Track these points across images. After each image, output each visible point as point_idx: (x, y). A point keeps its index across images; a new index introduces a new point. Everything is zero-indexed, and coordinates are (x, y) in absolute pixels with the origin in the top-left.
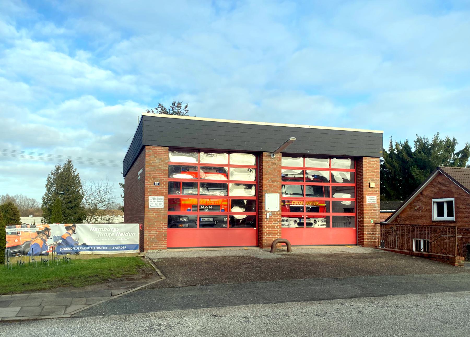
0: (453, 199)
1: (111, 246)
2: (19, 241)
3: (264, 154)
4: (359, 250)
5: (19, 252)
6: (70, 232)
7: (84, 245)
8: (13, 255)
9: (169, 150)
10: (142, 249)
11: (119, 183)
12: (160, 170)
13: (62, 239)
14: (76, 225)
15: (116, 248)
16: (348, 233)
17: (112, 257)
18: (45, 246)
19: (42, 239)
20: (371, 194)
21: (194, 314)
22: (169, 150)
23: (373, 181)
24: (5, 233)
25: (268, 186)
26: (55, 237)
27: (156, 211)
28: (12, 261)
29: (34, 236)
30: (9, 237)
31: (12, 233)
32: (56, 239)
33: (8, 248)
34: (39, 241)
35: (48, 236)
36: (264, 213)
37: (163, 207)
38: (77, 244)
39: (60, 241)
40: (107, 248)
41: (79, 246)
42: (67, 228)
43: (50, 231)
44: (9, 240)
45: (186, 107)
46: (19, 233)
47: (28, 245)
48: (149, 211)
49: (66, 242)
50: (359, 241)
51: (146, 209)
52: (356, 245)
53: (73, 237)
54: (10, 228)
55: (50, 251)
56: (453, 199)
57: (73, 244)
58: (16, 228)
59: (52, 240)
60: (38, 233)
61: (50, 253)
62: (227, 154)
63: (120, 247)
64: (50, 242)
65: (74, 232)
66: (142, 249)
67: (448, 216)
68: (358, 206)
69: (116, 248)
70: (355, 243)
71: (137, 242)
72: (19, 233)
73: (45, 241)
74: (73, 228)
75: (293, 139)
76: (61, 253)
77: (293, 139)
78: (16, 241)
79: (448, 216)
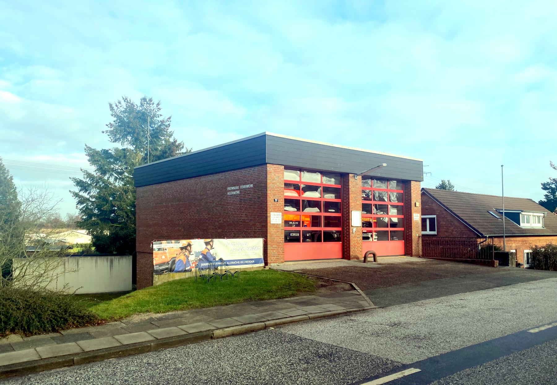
0: (435, 216)
1: (237, 260)
2: (166, 257)
3: (350, 175)
4: (344, 263)
5: (167, 269)
6: (209, 247)
7: (221, 260)
8: (160, 272)
9: (285, 169)
10: (266, 264)
11: (70, 191)
12: (278, 187)
13: (203, 254)
14: (214, 240)
15: (246, 262)
16: (398, 245)
17: (245, 272)
18: (188, 261)
19: (185, 255)
20: (416, 212)
21: (542, 282)
22: (285, 169)
23: (417, 201)
24: (152, 249)
25: (353, 204)
26: (196, 253)
27: (276, 226)
28: (158, 280)
29: (178, 253)
30: (156, 254)
31: (159, 249)
32: (197, 254)
33: (156, 265)
34: (182, 257)
35: (190, 252)
36: (351, 228)
37: (281, 223)
38: (215, 259)
39: (201, 257)
40: (238, 262)
41: (217, 261)
42: (207, 244)
43: (192, 246)
44: (156, 257)
45: (158, 104)
46: (166, 249)
47: (174, 262)
48: (270, 226)
49: (206, 257)
50: (408, 251)
51: (269, 224)
52: (342, 258)
53: (212, 252)
54: (157, 244)
55: (193, 267)
56: (435, 216)
57: (212, 259)
58: (161, 243)
59: (194, 256)
60: (182, 249)
61: (193, 269)
62: (299, 172)
63: (249, 262)
64: (192, 258)
65: (212, 247)
66: (266, 264)
67: (430, 231)
68: (407, 221)
69: (246, 262)
70: (403, 254)
71: (261, 255)
72: (166, 249)
73: (187, 257)
74: (211, 243)
75: (385, 165)
76: (202, 269)
77: (385, 165)
78: (163, 257)
79: (430, 231)
